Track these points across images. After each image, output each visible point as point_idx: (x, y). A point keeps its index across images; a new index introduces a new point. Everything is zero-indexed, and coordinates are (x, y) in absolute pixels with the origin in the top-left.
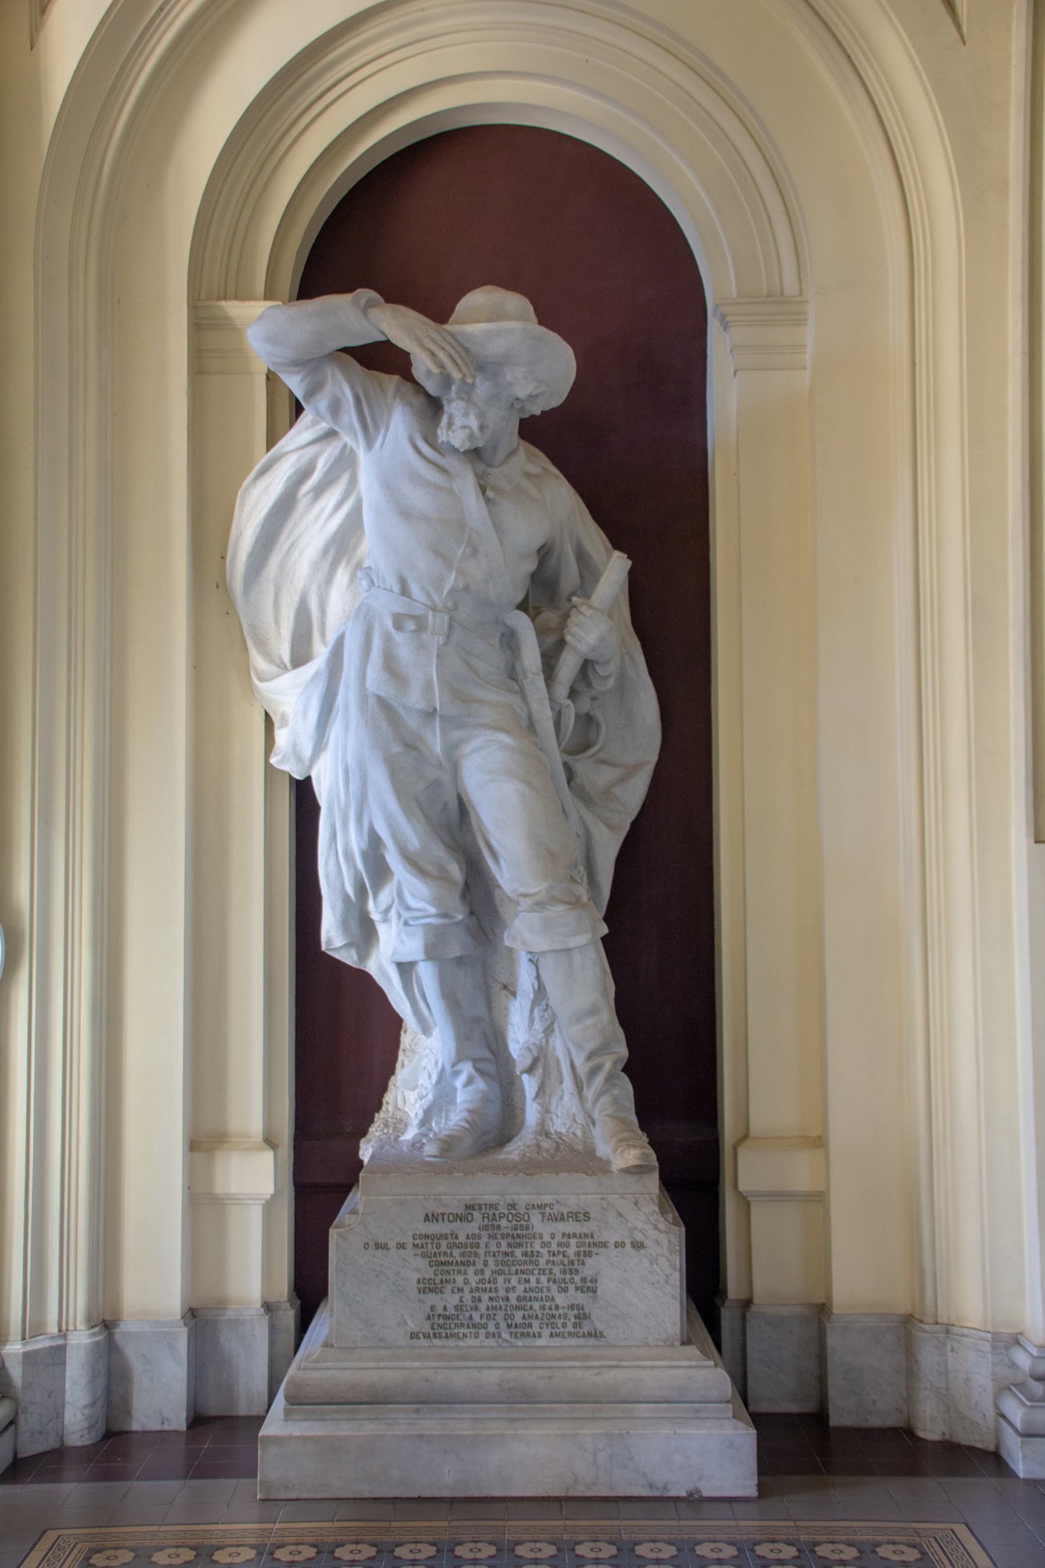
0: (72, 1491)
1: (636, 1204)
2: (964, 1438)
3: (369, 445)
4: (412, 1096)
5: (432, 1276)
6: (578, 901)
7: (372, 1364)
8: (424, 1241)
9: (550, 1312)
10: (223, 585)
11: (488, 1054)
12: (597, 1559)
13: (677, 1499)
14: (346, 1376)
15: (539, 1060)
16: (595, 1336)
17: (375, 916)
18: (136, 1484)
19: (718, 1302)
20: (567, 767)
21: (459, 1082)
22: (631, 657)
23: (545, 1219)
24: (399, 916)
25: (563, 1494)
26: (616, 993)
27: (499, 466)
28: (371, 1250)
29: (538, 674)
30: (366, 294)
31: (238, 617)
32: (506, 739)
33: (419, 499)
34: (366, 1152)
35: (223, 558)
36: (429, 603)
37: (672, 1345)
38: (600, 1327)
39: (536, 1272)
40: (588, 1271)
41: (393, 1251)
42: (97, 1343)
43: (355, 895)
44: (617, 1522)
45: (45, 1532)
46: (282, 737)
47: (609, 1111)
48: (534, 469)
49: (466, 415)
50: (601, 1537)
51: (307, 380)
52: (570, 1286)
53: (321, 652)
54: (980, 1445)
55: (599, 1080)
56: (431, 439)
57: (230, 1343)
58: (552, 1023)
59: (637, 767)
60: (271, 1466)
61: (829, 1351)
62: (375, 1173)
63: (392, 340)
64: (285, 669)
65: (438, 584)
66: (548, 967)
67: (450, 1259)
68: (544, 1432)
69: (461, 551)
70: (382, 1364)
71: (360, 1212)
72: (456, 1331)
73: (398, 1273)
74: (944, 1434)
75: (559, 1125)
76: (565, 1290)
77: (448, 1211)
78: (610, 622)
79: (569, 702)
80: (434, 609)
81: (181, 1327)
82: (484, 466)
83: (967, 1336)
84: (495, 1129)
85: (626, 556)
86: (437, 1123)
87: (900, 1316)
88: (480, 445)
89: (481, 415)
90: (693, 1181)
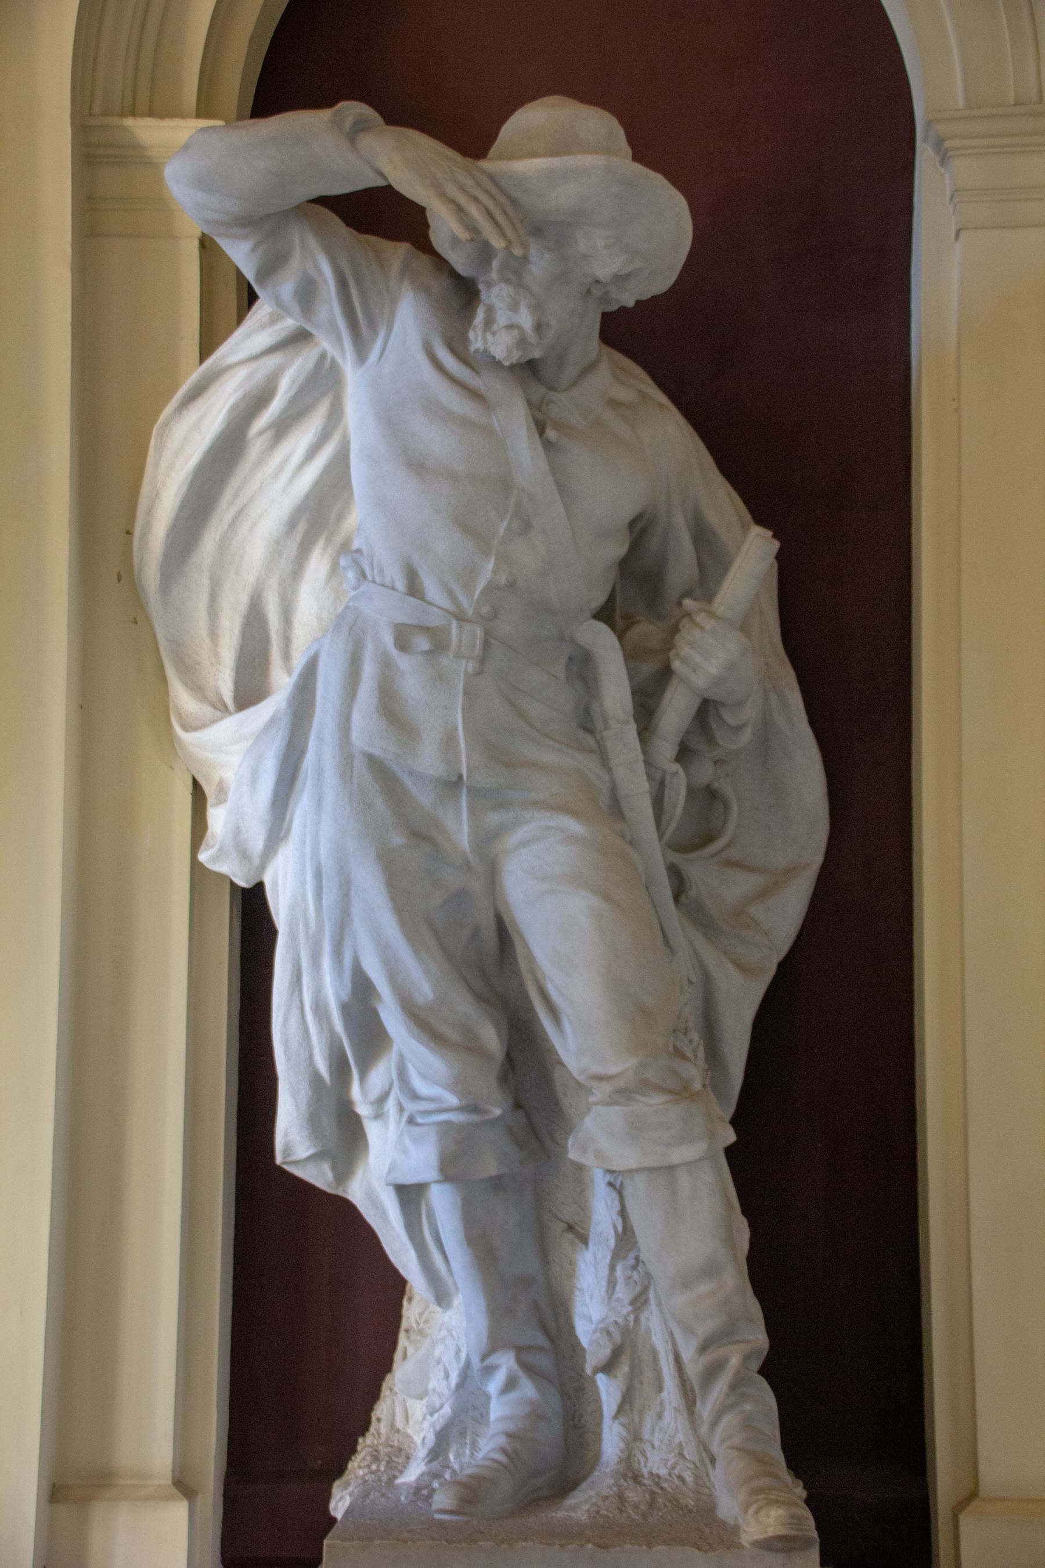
4: (417, 1408)
6: (686, 1088)
10: (128, 576)
11: (541, 1340)
15: (626, 1349)
17: (363, 1109)
20: (676, 874)
21: (494, 1385)
24: (401, 1109)
30: (353, 110)
31: (152, 627)
32: (574, 826)
33: (437, 441)
34: (340, 1503)
36: (451, 608)
43: (331, 1076)
46: (217, 818)
47: (737, 1440)
48: (624, 394)
49: (514, 307)
53: (283, 683)
55: (720, 1386)
56: (458, 347)
58: (645, 1289)
62: (350, 1539)
64: (225, 711)
66: (637, 1190)
69: (504, 524)
75: (655, 1462)
79: (676, 767)
80: (460, 617)
82: (543, 390)
84: (553, 1463)
85: (770, 533)
86: (458, 1456)
89: (537, 307)
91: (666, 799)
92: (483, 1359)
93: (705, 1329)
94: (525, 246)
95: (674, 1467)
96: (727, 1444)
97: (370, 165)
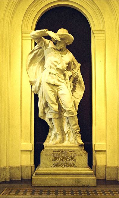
40: (75, 159)
41: (49, 155)
63: (49, 35)
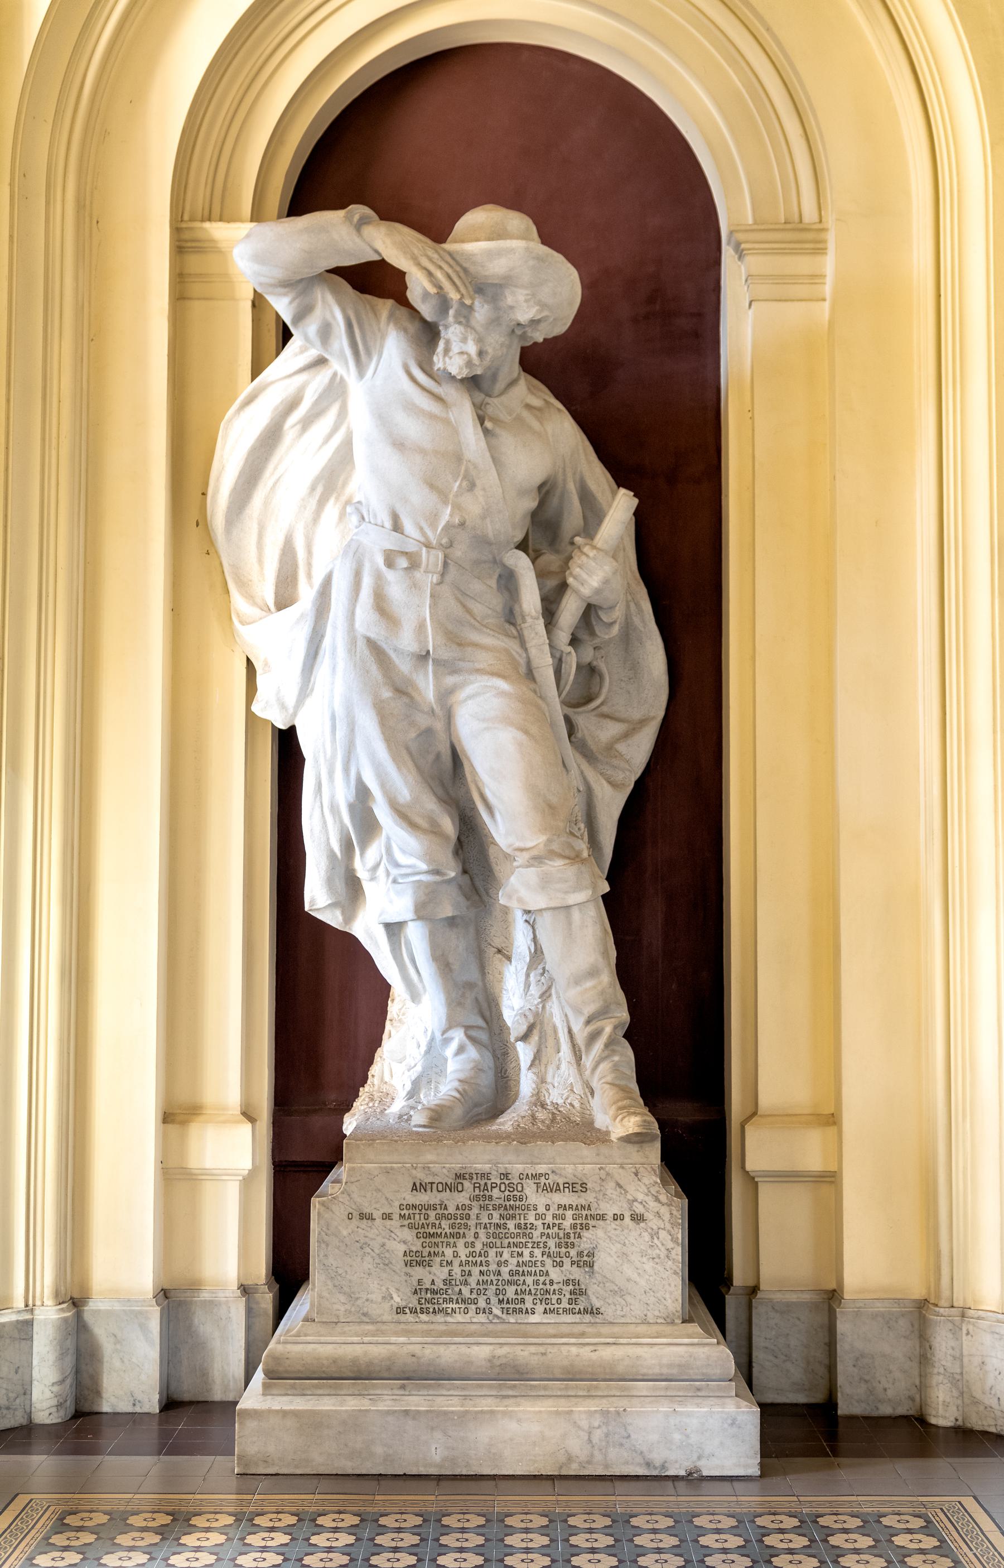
0: (41, 1464)
1: (636, 1174)
2: (977, 1423)
3: (361, 368)
4: (398, 1069)
5: (420, 1248)
6: (577, 856)
7: (355, 1339)
8: (411, 1211)
9: (545, 1287)
10: (203, 523)
11: (480, 1022)
12: (590, 1529)
13: (676, 1478)
14: (326, 1351)
16: (592, 1313)
17: (362, 873)
18: (107, 1458)
19: (723, 1290)
20: (568, 720)
22: (637, 605)
23: (540, 1190)
25: (556, 1473)
26: (617, 958)
27: (497, 396)
28: (355, 1221)
29: (538, 618)
30: (359, 210)
31: (219, 557)
33: (413, 429)
34: (349, 1124)
35: (203, 494)
36: (422, 539)
37: (673, 1323)
38: (597, 1303)
39: (530, 1245)
40: (585, 1245)
41: (378, 1221)
42: (65, 1320)
44: (613, 1498)
45: (17, 1495)
47: (609, 1079)
48: (536, 402)
49: (464, 340)
50: (595, 1510)
51: (297, 301)
52: (565, 1260)
53: (307, 593)
54: (993, 1430)
55: (599, 1045)
56: (426, 366)
57: (204, 1325)
58: (550, 988)
59: (643, 722)
60: (250, 1441)
61: (839, 1337)
62: (361, 1140)
63: (386, 259)
65: (433, 518)
66: (545, 925)
67: (439, 1231)
68: (537, 1409)
69: (457, 484)
70: (366, 1339)
71: (344, 1181)
72: (444, 1306)
73: (383, 1245)
74: (957, 1420)
75: (555, 1096)
76: (561, 1264)
77: (437, 1180)
78: (615, 564)
79: (570, 649)
80: (428, 546)
81: (152, 1306)
82: (482, 396)
83: (983, 1319)
84: (489, 1098)
85: (632, 494)
87: (915, 1301)
88: (479, 373)
89: (480, 340)
90: (698, 1155)
91: (563, 671)
92: (442, 1035)
93: (589, 1009)
94: (473, 299)
95: (567, 1099)
96: (603, 1081)
97: (371, 247)
